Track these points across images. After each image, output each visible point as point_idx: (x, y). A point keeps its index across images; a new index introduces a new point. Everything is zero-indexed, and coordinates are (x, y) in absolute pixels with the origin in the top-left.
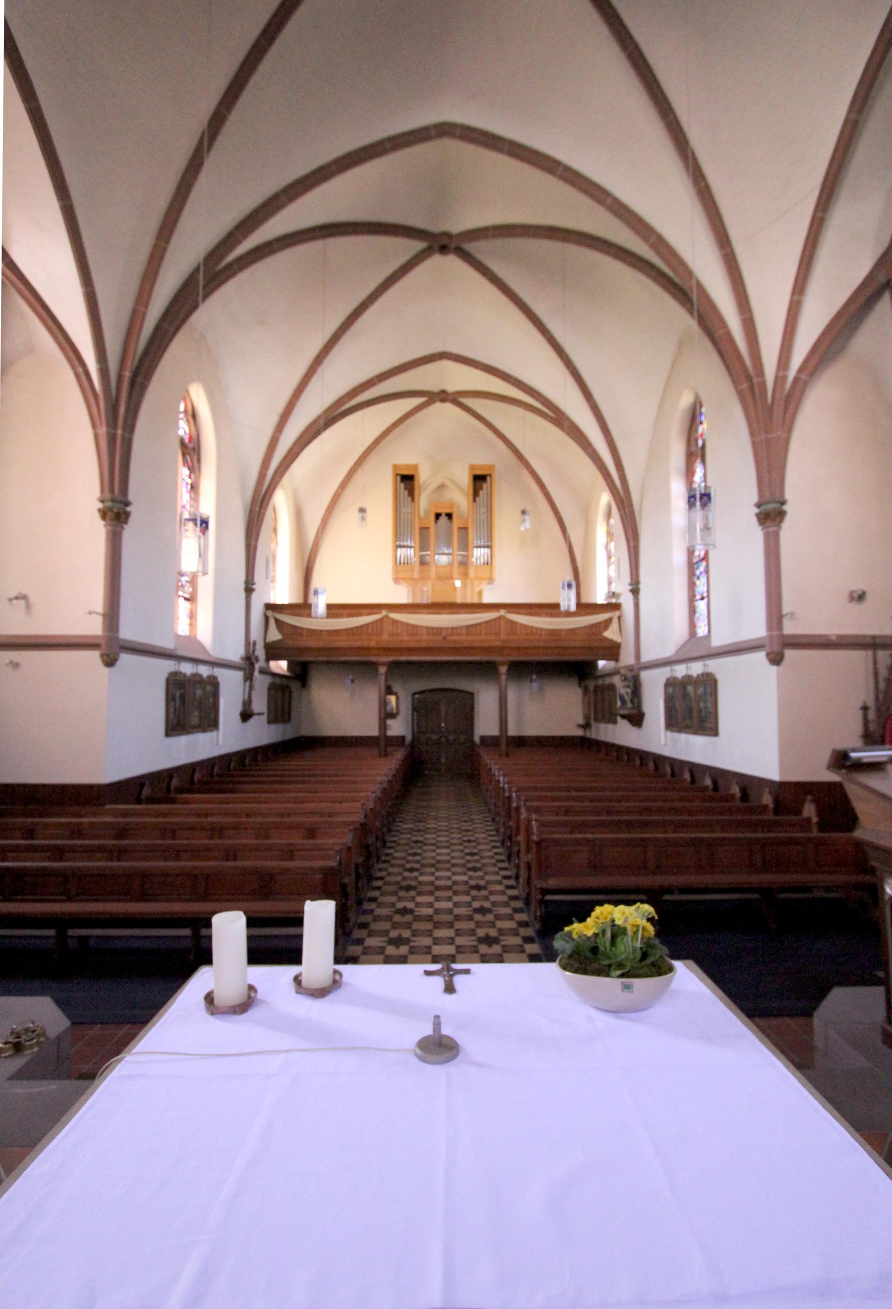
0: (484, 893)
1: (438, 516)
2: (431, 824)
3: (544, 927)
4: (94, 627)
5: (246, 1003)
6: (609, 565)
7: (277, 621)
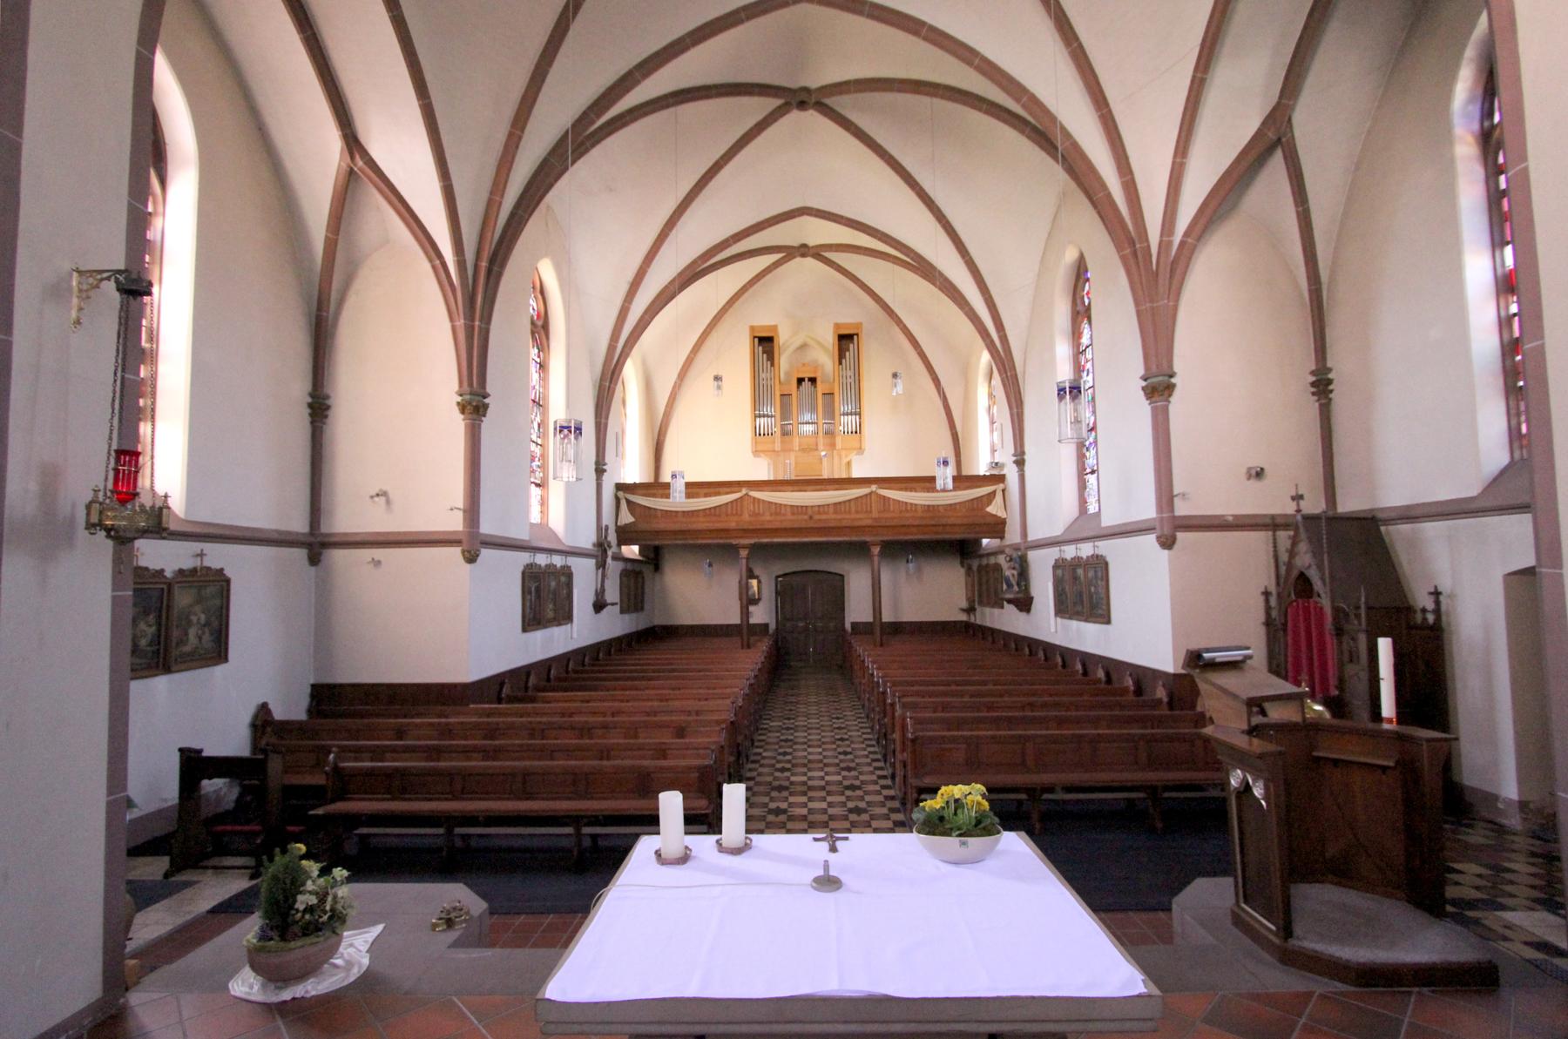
0: (859, 793)
1: (800, 381)
2: (801, 722)
3: (904, 808)
4: (454, 523)
5: (684, 859)
6: (992, 431)
7: (628, 502)
